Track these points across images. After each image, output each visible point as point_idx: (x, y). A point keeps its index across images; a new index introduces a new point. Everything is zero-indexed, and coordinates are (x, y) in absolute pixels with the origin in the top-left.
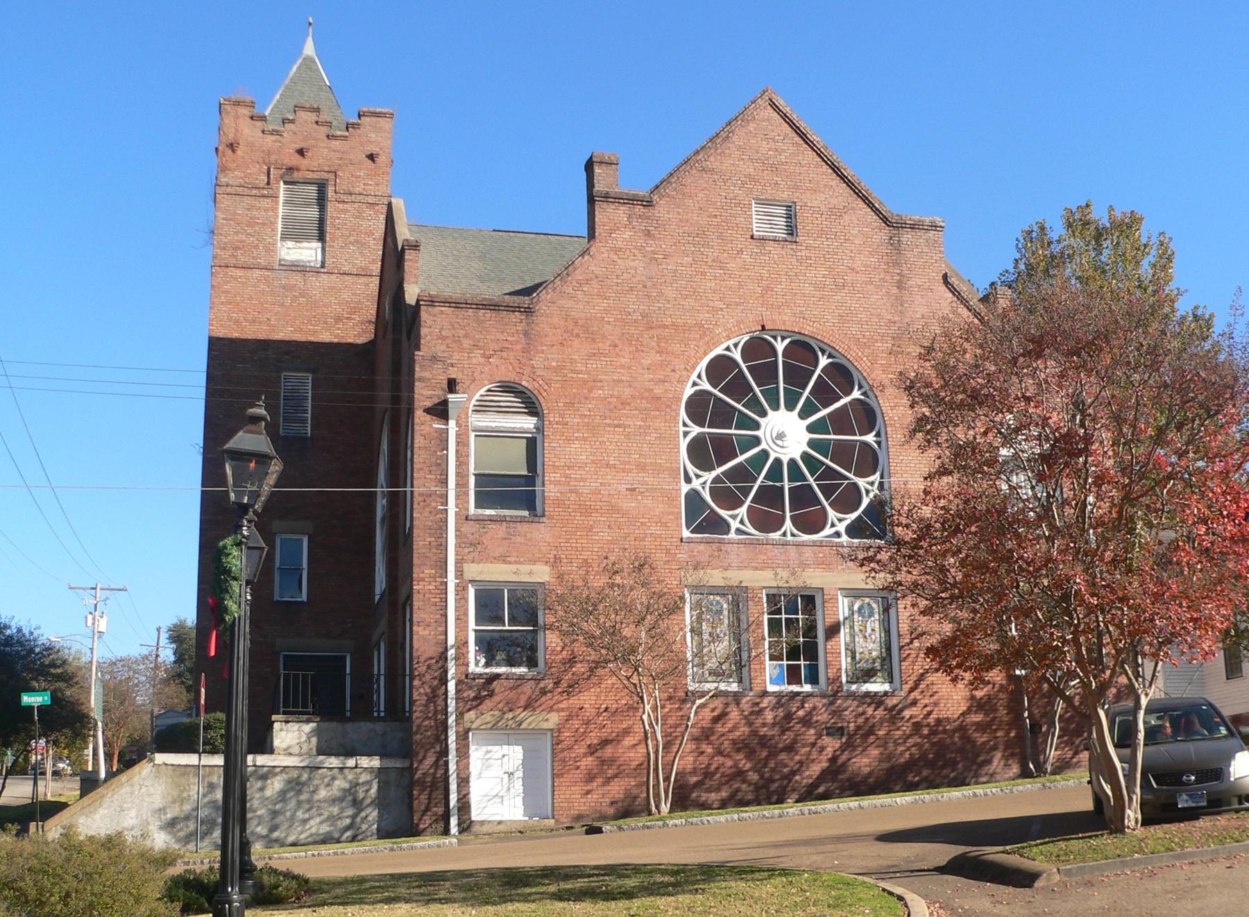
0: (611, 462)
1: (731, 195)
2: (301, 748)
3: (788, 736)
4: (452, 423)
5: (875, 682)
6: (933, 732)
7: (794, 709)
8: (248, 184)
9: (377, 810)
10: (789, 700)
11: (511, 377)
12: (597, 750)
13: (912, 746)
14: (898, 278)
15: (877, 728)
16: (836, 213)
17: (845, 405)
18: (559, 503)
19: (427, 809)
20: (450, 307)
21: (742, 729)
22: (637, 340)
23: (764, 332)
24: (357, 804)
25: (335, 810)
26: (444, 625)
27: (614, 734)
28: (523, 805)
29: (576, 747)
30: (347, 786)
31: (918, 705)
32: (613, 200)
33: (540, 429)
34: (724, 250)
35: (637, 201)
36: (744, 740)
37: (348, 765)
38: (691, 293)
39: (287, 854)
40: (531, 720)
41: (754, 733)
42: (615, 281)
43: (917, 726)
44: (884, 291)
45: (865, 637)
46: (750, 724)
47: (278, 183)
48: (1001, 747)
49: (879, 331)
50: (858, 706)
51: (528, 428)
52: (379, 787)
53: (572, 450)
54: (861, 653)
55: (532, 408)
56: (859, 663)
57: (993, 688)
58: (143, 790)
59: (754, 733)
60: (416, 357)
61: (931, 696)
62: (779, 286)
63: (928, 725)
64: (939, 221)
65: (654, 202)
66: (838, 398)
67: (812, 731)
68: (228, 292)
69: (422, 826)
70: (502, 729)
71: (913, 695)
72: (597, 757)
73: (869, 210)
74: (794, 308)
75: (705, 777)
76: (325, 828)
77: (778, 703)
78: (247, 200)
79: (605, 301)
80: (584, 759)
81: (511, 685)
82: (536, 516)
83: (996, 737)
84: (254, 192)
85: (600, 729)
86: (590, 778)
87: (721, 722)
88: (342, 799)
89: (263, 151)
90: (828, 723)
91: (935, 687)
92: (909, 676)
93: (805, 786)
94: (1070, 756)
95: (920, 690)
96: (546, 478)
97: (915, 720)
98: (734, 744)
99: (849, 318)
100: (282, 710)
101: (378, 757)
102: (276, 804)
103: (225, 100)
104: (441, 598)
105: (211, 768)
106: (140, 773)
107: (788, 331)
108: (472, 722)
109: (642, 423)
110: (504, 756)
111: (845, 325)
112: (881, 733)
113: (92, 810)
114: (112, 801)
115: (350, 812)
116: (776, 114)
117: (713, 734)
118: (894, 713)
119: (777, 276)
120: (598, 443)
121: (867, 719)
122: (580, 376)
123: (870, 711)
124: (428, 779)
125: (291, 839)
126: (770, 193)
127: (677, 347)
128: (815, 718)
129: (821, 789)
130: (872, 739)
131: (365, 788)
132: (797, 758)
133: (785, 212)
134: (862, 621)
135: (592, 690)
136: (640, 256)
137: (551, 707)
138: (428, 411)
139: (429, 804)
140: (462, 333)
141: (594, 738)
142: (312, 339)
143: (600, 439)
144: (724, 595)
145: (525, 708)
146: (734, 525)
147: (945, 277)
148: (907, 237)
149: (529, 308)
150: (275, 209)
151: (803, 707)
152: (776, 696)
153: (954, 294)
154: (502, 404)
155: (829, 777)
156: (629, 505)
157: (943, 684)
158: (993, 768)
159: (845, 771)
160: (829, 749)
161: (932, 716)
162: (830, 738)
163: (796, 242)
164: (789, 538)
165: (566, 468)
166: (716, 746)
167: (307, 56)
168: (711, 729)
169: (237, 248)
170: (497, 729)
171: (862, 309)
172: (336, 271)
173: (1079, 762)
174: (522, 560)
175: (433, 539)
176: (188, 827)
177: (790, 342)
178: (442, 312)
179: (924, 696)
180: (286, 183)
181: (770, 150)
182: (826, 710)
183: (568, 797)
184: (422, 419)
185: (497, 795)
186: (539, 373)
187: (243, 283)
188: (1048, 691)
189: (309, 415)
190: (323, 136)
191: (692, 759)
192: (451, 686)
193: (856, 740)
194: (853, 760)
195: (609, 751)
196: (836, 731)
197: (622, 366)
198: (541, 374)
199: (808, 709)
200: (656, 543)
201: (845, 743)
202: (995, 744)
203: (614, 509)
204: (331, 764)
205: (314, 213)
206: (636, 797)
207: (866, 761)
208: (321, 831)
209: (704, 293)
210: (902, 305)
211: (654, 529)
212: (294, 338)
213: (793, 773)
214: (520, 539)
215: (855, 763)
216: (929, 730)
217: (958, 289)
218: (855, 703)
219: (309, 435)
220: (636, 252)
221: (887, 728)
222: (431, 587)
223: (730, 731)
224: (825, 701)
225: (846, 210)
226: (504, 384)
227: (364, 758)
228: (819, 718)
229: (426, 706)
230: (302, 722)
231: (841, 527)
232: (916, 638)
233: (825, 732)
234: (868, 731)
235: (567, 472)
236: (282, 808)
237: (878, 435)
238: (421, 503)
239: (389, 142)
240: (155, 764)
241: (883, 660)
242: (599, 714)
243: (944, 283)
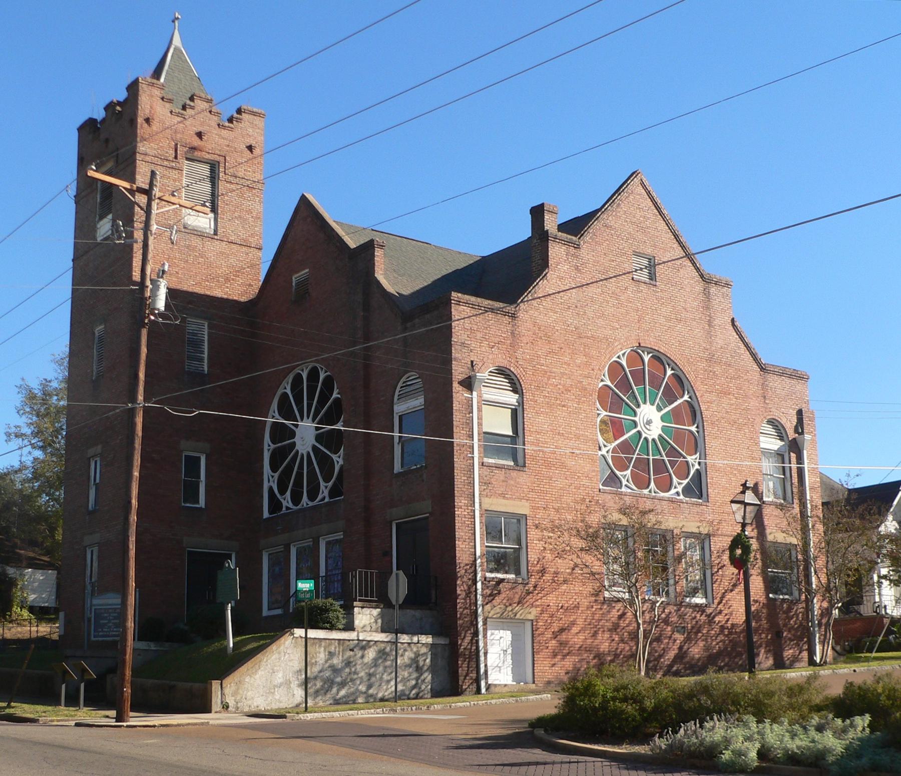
2: (371, 627)
4: (475, 393)
5: (698, 597)
6: (730, 633)
8: (161, 155)
9: (431, 675)
11: (504, 363)
12: (557, 635)
14: (708, 318)
17: (680, 404)
19: (467, 675)
20: (469, 307)
21: (633, 625)
24: (419, 669)
26: (473, 541)
27: (566, 625)
28: (512, 673)
29: (546, 633)
30: (413, 656)
33: (521, 403)
39: (459, 704)
43: (722, 628)
53: (540, 420)
55: (516, 388)
57: (759, 605)
58: (286, 657)
60: (452, 343)
63: (727, 628)
67: (669, 628)
69: (464, 687)
70: (506, 618)
72: (558, 641)
73: (693, 268)
75: (615, 657)
80: (550, 642)
81: (510, 587)
82: (518, 466)
84: (166, 163)
85: (559, 621)
86: (555, 655)
87: (623, 619)
88: (410, 666)
91: (731, 602)
96: (526, 440)
98: (630, 635)
100: (358, 598)
101: (431, 636)
102: (370, 668)
103: (142, 80)
104: (472, 522)
105: (330, 641)
106: (284, 644)
108: (489, 612)
109: (577, 406)
110: (501, 638)
113: (254, 671)
114: (267, 665)
115: (415, 675)
118: (710, 619)
121: (697, 622)
122: (543, 367)
125: (380, 695)
128: (670, 619)
135: (554, 593)
137: (532, 604)
138: (461, 383)
141: (556, 627)
142: (208, 293)
148: (713, 289)
149: (514, 314)
155: (678, 660)
156: (570, 463)
159: (687, 657)
161: (729, 622)
163: (656, 286)
168: (618, 623)
170: (502, 618)
172: (226, 240)
173: (802, 658)
174: (514, 497)
175: (466, 478)
176: (315, 685)
182: (676, 614)
183: (542, 668)
184: (457, 389)
185: (497, 666)
189: (206, 356)
190: (214, 124)
191: (607, 644)
192: (479, 585)
194: (690, 650)
195: (564, 637)
198: (521, 363)
199: (667, 613)
204: (404, 639)
205: (207, 187)
206: (579, 670)
209: (608, 316)
210: (711, 338)
212: (195, 291)
213: (661, 656)
214: (512, 482)
219: (206, 372)
222: (466, 513)
227: (423, 636)
229: (465, 599)
230: (372, 608)
231: (680, 489)
232: (720, 568)
235: (537, 436)
236: (374, 672)
237: (697, 427)
238: (459, 451)
239: (262, 138)
240: (294, 637)
241: (702, 582)
242: (558, 611)
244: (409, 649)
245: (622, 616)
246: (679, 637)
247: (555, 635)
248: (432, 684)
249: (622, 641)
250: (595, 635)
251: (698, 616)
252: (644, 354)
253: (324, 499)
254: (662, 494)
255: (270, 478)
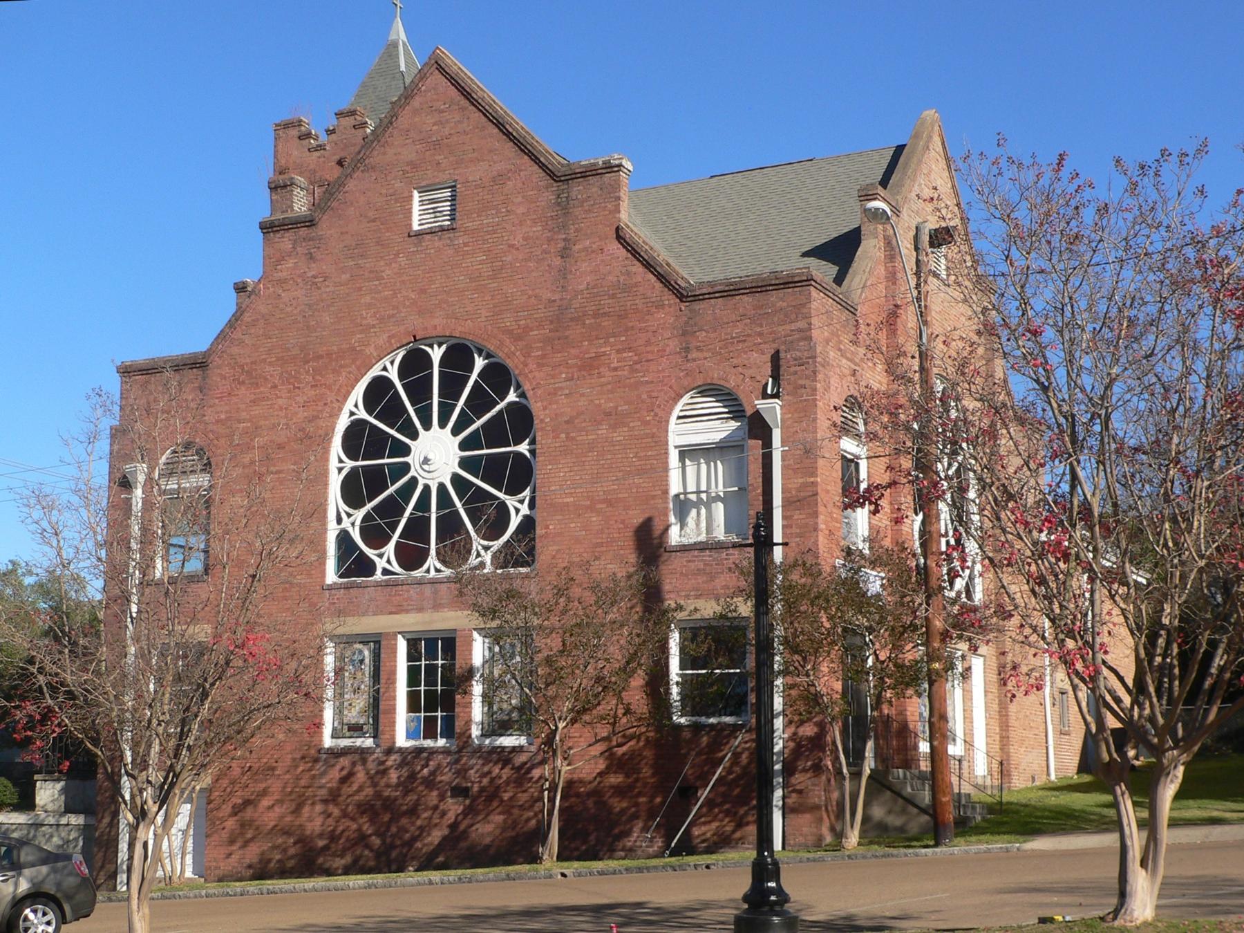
67: (435, 793)
86: (232, 842)
121: (492, 780)
128: (439, 778)
195: (249, 813)
213: (415, 839)
242: (243, 774)
244: (55, 834)
245: (344, 780)
246: (454, 807)
247: (236, 811)
249: (345, 815)
250: (297, 811)
251: (496, 771)
255: (344, 516)
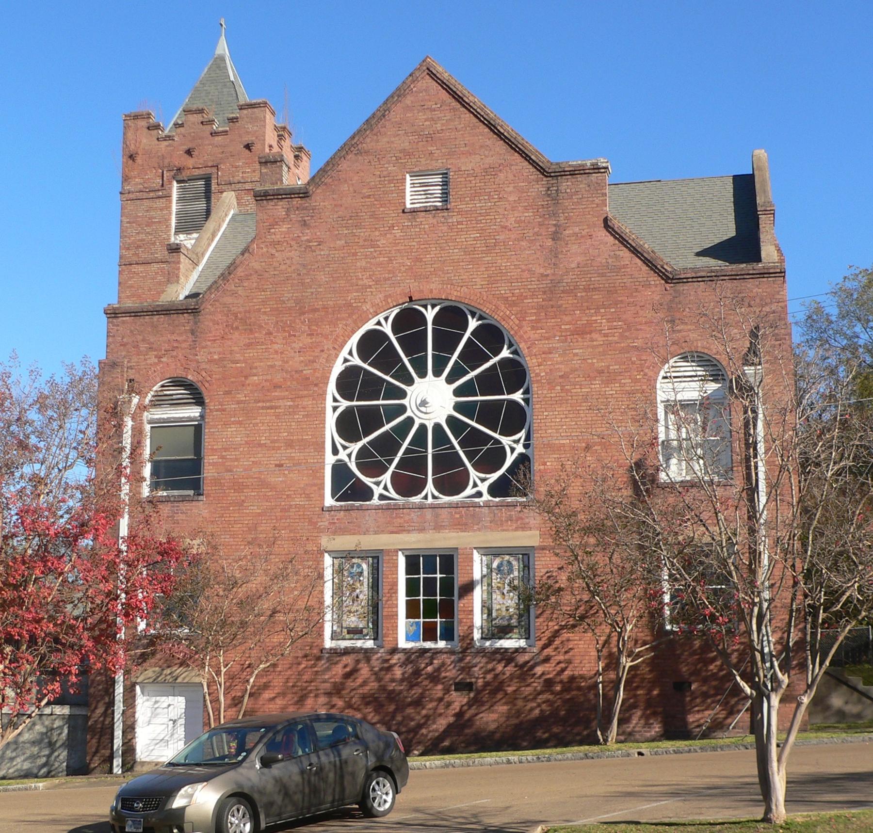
0: (262, 442)
1: (385, 173)
3: (417, 691)
5: (510, 638)
7: (423, 666)
10: (418, 657)
11: (180, 373)
13: (544, 702)
15: (506, 684)
16: (491, 171)
18: (217, 482)
20: (130, 316)
22: (290, 326)
23: (413, 303)
24: (51, 745)
25: (35, 750)
27: (256, 688)
30: (44, 730)
31: (551, 661)
32: (272, 197)
34: (376, 228)
35: (294, 194)
36: (374, 694)
37: (45, 713)
38: (342, 275)
40: (186, 675)
41: (383, 688)
42: (272, 273)
43: (549, 684)
44: (538, 244)
45: (503, 594)
46: (379, 680)
47: (170, 183)
48: (642, 705)
49: (529, 287)
50: (487, 663)
51: (195, 417)
52: (69, 731)
53: (228, 433)
54: (497, 610)
55: (198, 400)
56: (495, 619)
59: (383, 688)
61: (566, 652)
62: (428, 256)
64: (602, 162)
65: (311, 192)
66: (488, 359)
67: (440, 687)
68: (132, 287)
69: (92, 766)
70: (162, 683)
71: (547, 652)
73: (527, 163)
74: (443, 276)
76: (26, 766)
77: (407, 659)
78: (146, 203)
79: (263, 293)
83: (635, 696)
84: (152, 195)
87: (353, 677)
89: (158, 157)
90: (456, 678)
92: (543, 632)
93: (431, 739)
94: (723, 716)
95: (554, 646)
97: (548, 676)
99: (498, 278)
101: (68, 706)
107: (435, 299)
110: (169, 705)
111: (494, 286)
112: (510, 689)
115: (46, 752)
116: (435, 82)
117: (343, 689)
119: (427, 246)
120: (251, 425)
121: (496, 676)
122: (238, 365)
123: (500, 668)
124: (99, 726)
126: (424, 163)
127: (327, 329)
129: (446, 743)
130: (499, 696)
131: (59, 732)
132: (424, 712)
133: (441, 180)
134: (501, 579)
136: (295, 246)
139: (98, 746)
140: (140, 338)
143: (253, 421)
144: (362, 558)
145: (181, 665)
146: (378, 491)
147: (606, 220)
148: (566, 184)
150: (169, 208)
151: (431, 663)
152: (406, 653)
153: (615, 238)
154: (174, 397)
156: (276, 479)
157: (580, 640)
158: (631, 726)
160: (456, 704)
162: (459, 693)
163: (447, 209)
164: (430, 500)
165: (223, 450)
166: (347, 699)
167: (219, 55)
169: (139, 247)
170: (157, 682)
171: (513, 267)
177: (441, 309)
178: (124, 322)
179: (559, 652)
180: (178, 182)
181: (426, 120)
182: (454, 667)
185: (163, 739)
186: (203, 366)
187: (143, 277)
188: (700, 647)
193: (485, 695)
194: (481, 715)
196: (463, 686)
197: (276, 352)
200: (299, 513)
201: (473, 698)
202: (635, 702)
203: (264, 484)
207: (493, 716)
208: (25, 767)
211: (298, 501)
213: (420, 726)
215: (482, 718)
216: (562, 687)
217: (619, 232)
218: (484, 660)
220: (293, 243)
221: (518, 685)
223: (361, 686)
224: (453, 657)
225: (501, 168)
226: (174, 380)
227: (57, 706)
228: (447, 674)
233: (453, 688)
234: (496, 687)
241: (520, 616)
242: (243, 670)
243: (605, 227)
244: (38, 722)
248: (68, 761)
252: (426, 309)
253: (479, 494)
254: (446, 499)
